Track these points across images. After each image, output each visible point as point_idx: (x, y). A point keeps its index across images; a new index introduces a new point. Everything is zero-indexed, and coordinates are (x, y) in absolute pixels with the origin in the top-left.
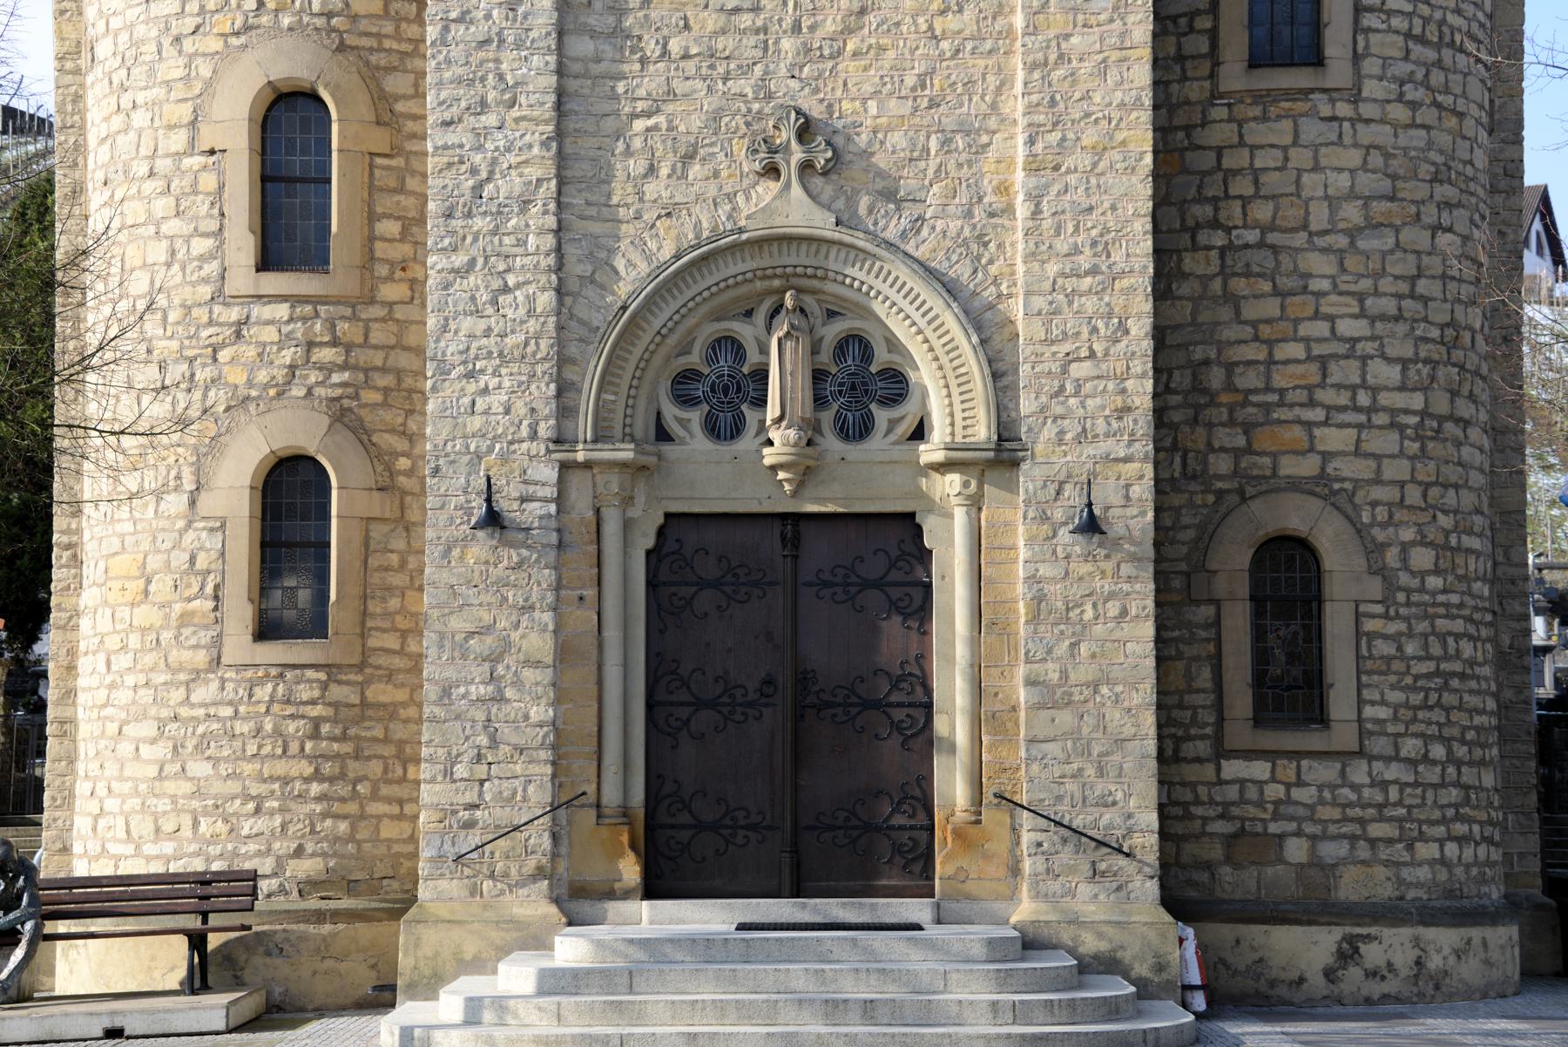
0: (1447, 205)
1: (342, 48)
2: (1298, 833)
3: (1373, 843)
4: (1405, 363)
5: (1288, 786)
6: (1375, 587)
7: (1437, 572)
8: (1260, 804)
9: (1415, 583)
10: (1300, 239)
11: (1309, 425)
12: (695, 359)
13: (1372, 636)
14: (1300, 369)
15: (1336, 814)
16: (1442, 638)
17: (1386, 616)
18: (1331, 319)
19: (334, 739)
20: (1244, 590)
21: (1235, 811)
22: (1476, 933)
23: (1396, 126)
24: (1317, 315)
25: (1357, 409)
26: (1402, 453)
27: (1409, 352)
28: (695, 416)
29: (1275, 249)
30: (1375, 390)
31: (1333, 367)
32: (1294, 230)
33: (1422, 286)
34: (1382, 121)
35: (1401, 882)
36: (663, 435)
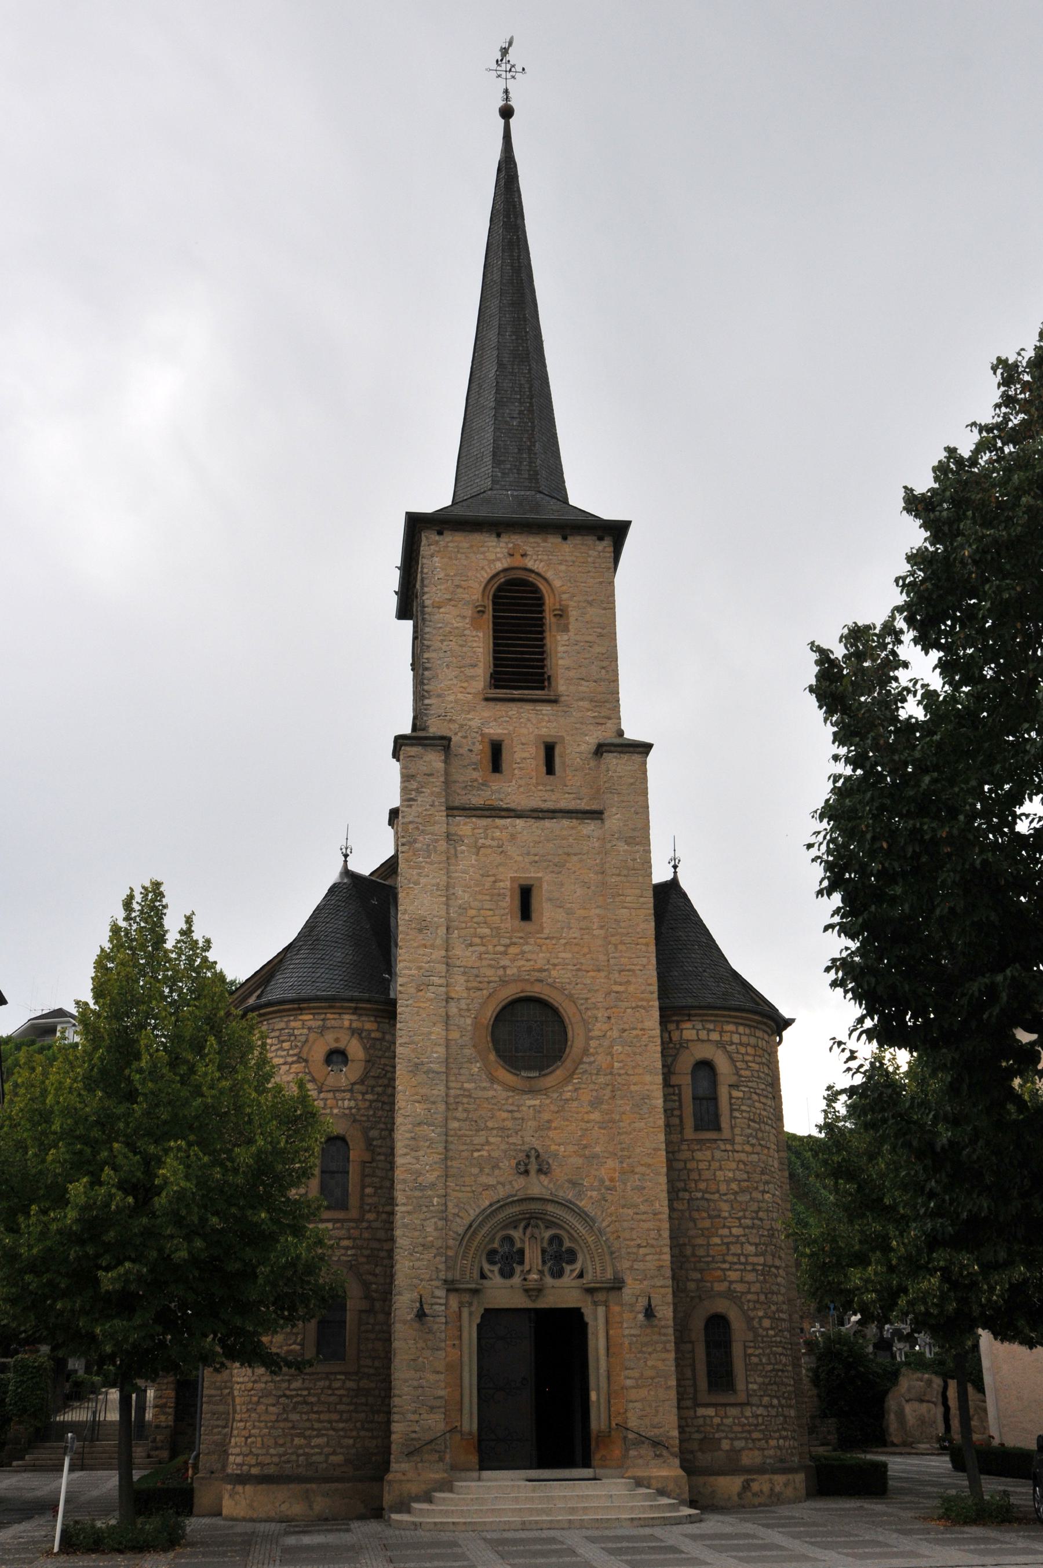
0: (767, 1183)
1: (355, 1121)
2: (726, 1438)
3: (754, 1440)
4: (756, 1245)
5: (722, 1418)
6: (750, 1336)
7: (772, 1329)
8: (712, 1426)
9: (765, 1333)
10: (717, 1196)
11: (724, 1270)
12: (496, 1245)
13: (750, 1355)
14: (719, 1248)
15: (740, 1429)
16: (775, 1354)
17: (755, 1347)
18: (729, 1228)
19: (348, 1404)
20: (702, 1338)
21: (702, 1429)
22: (790, 1476)
23: (747, 1152)
24: (724, 1226)
25: (741, 1264)
26: (758, 1281)
27: (757, 1241)
28: (496, 1268)
29: (707, 1200)
30: (746, 1256)
31: (732, 1247)
32: (714, 1193)
33: (761, 1214)
34: (742, 1152)
35: (764, 1456)
36: (483, 1276)
